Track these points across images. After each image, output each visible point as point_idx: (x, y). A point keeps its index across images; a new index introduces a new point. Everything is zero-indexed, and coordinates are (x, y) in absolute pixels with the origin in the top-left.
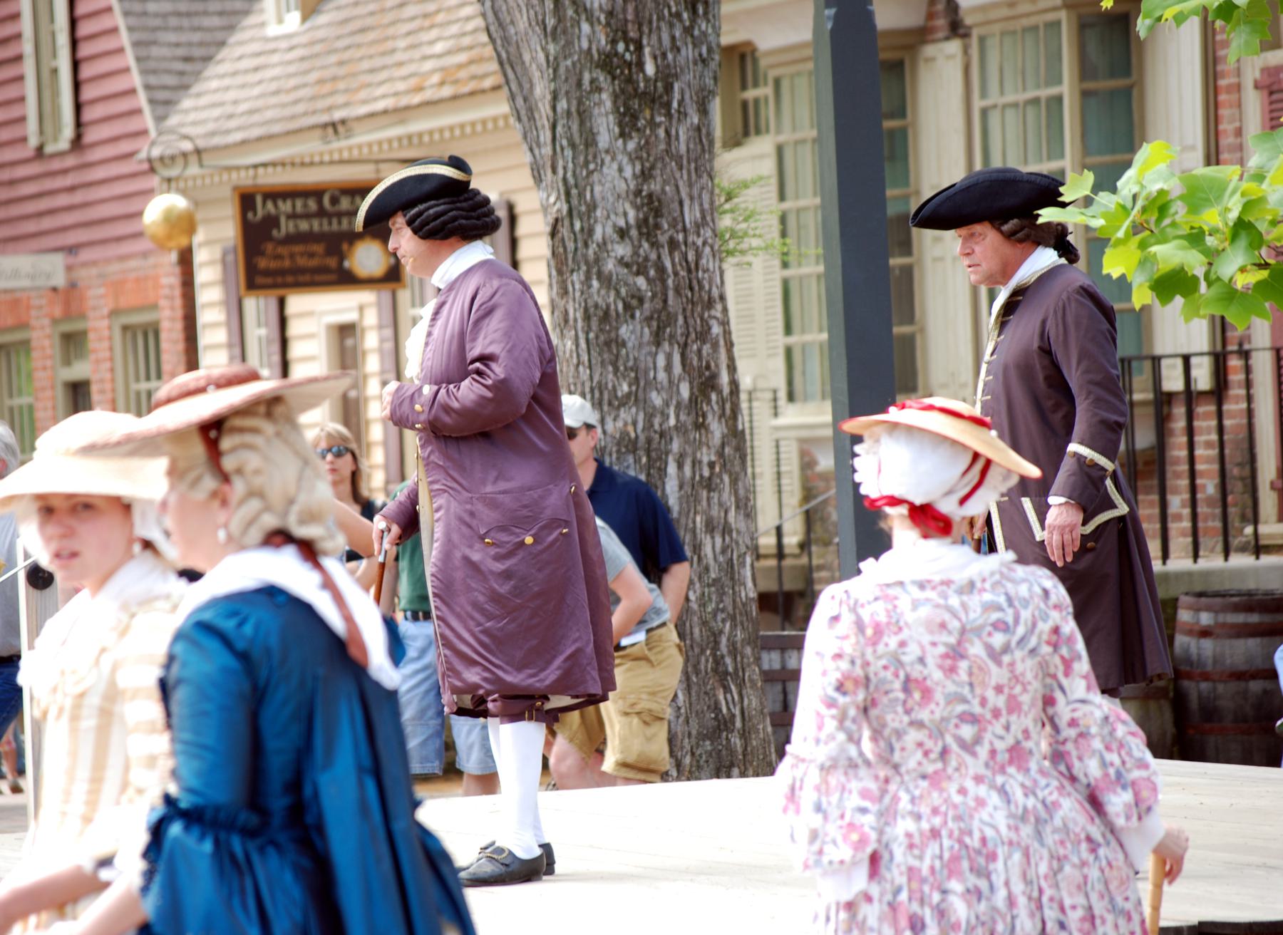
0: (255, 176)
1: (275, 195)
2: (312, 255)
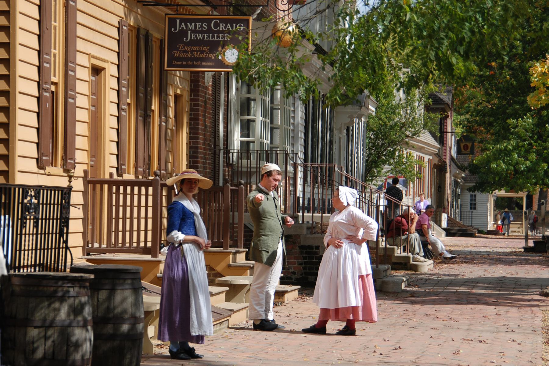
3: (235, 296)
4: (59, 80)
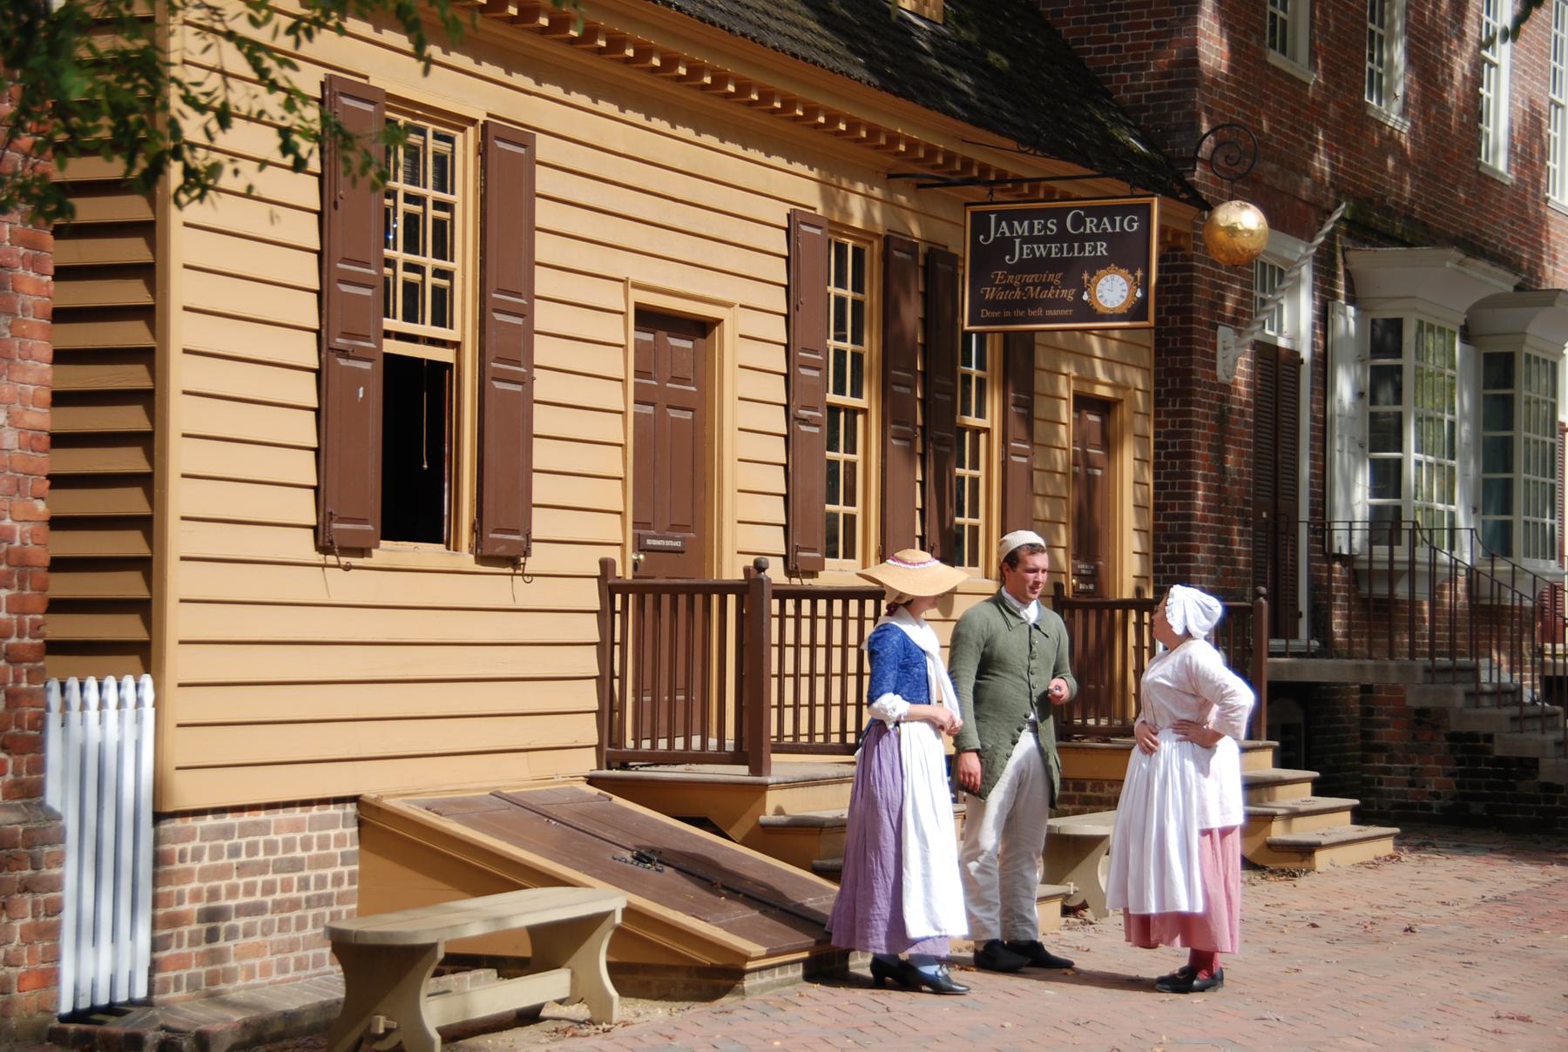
0: (991, 193)
3: (1077, 863)
4: (463, 335)
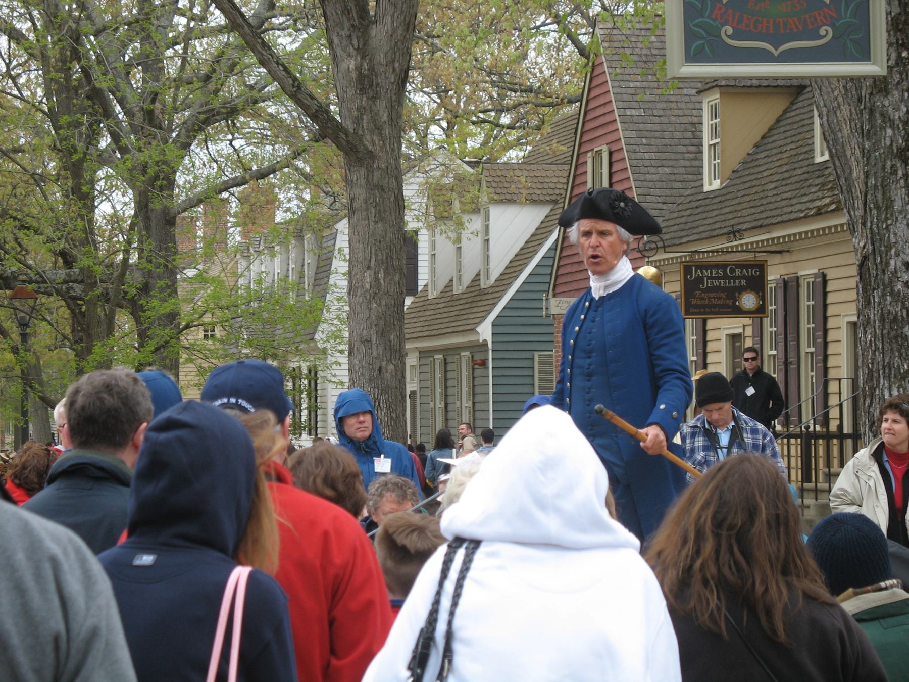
1: (702, 267)
2: (719, 298)
